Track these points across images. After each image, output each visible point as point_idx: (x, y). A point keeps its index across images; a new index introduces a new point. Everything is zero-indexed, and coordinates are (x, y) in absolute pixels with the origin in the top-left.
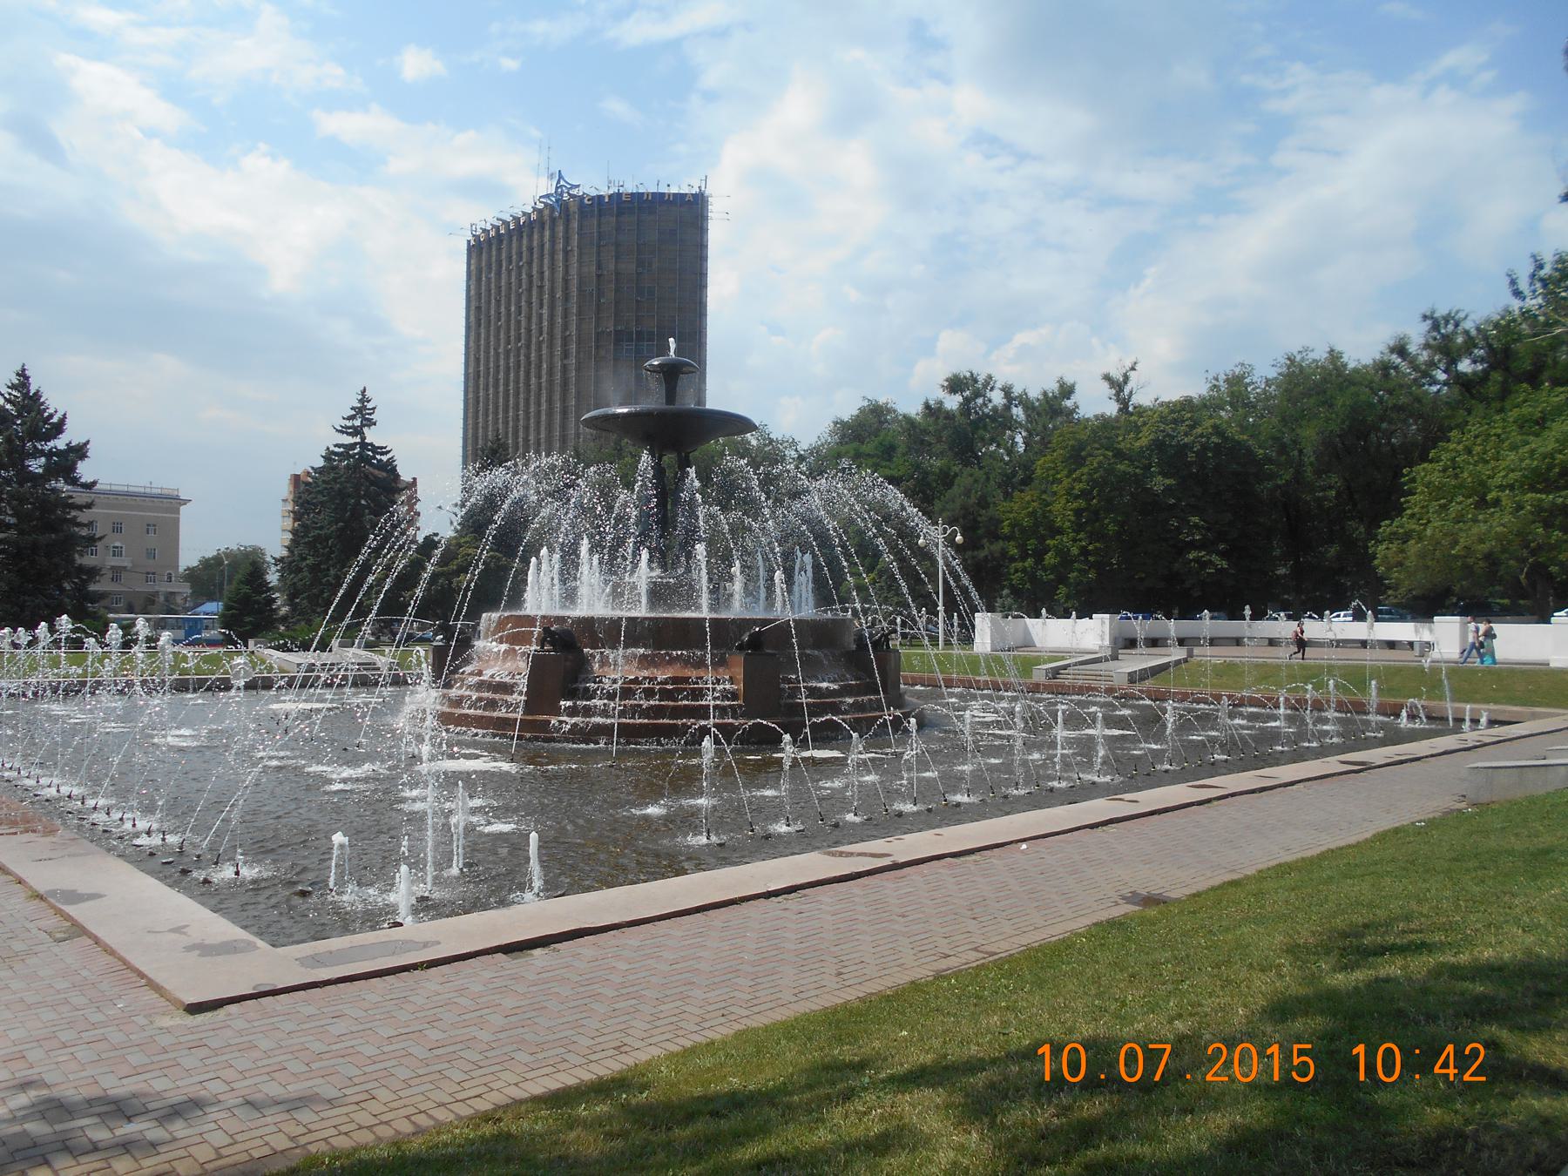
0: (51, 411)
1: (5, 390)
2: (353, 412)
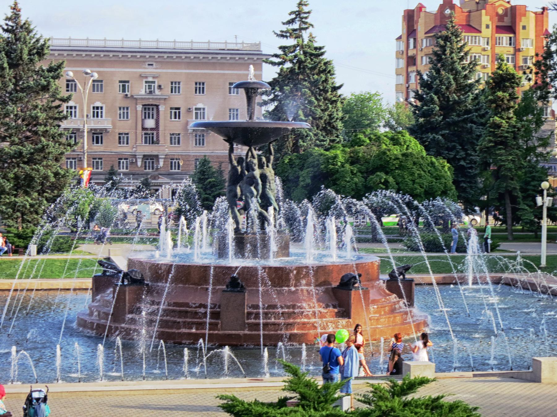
0: (38, 36)
1: (3, 23)
2: (293, 16)
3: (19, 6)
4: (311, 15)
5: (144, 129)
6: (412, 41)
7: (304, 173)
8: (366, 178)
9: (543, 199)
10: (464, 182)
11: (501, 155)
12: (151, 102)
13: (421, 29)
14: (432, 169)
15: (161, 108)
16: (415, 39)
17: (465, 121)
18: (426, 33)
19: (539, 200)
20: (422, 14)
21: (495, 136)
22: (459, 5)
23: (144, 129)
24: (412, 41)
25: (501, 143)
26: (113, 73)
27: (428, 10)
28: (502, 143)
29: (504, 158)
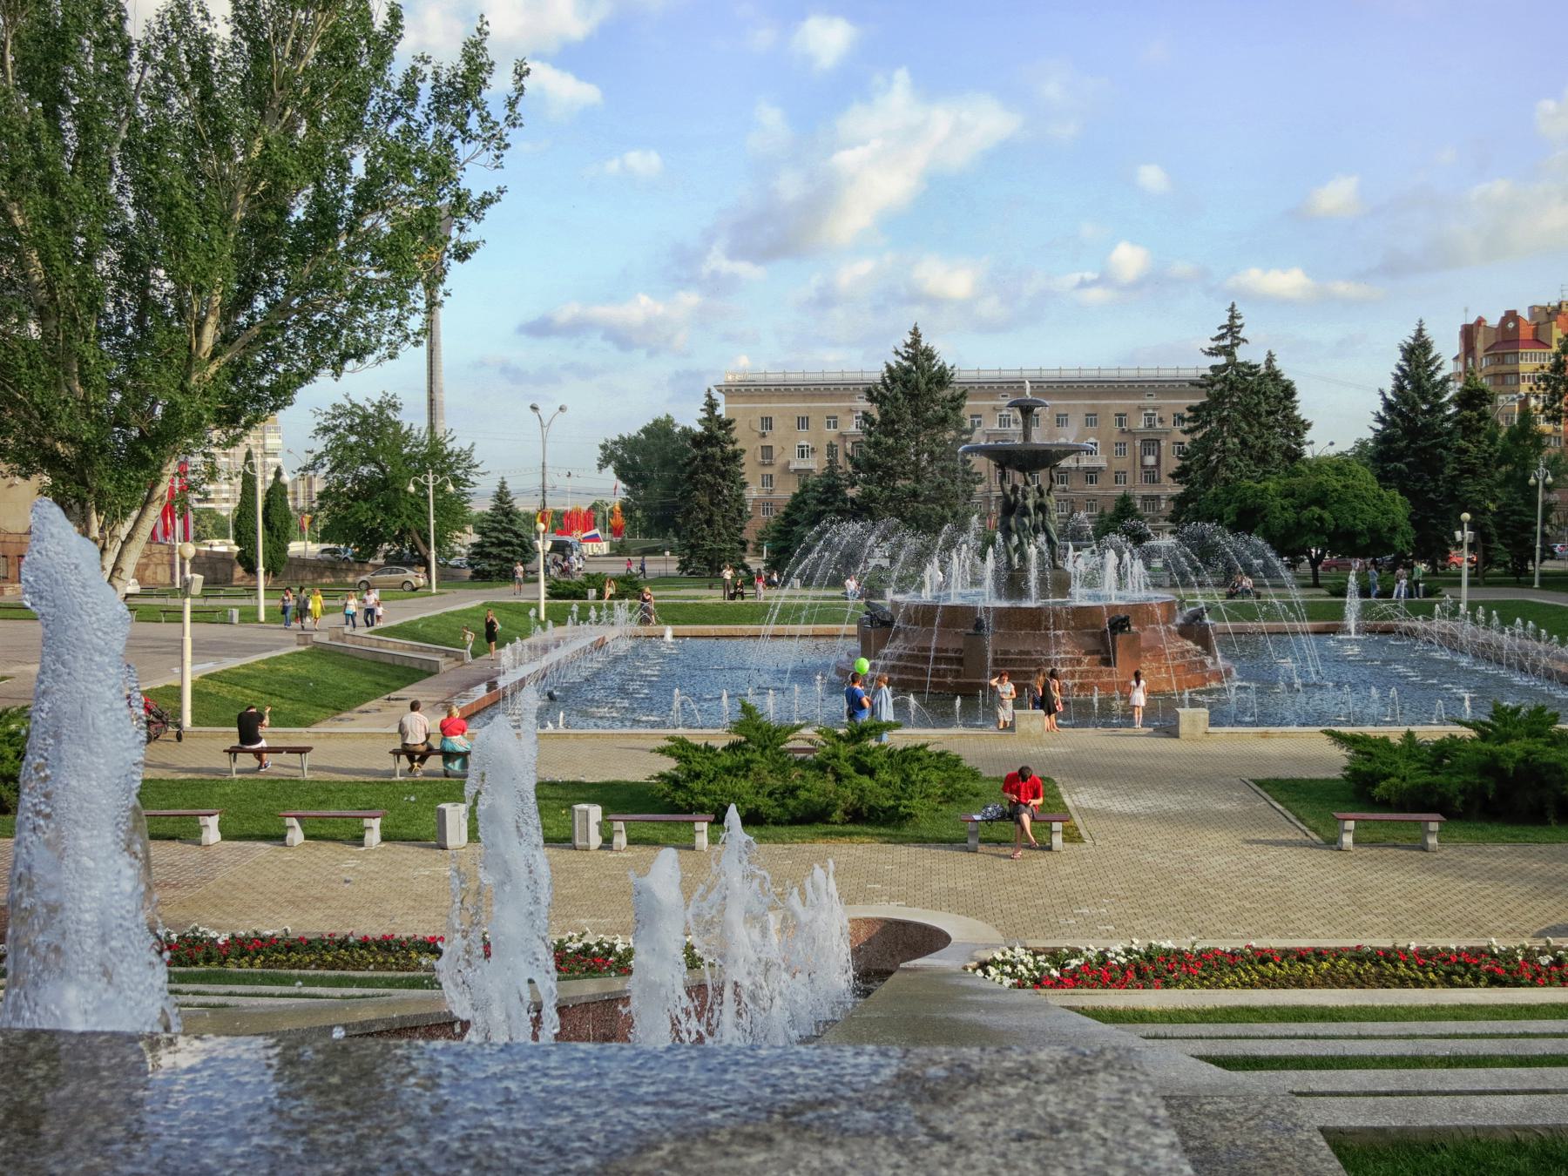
2: (1225, 331)
3: (920, 331)
4: (1243, 330)
5: (1143, 466)
6: (1470, 361)
7: (1228, 509)
8: (1298, 513)
9: (1463, 532)
10: (1433, 518)
11: (1468, 485)
12: (1151, 437)
13: (1480, 346)
14: (1380, 503)
15: (1163, 444)
16: (1474, 359)
17: (1435, 446)
18: (1486, 351)
19: (1458, 534)
20: (1481, 330)
21: (1461, 462)
22: (1527, 318)
23: (1143, 466)
24: (1470, 361)
25: (1468, 471)
26: (1107, 406)
27: (1489, 324)
28: (1472, 471)
29: (1470, 488)
